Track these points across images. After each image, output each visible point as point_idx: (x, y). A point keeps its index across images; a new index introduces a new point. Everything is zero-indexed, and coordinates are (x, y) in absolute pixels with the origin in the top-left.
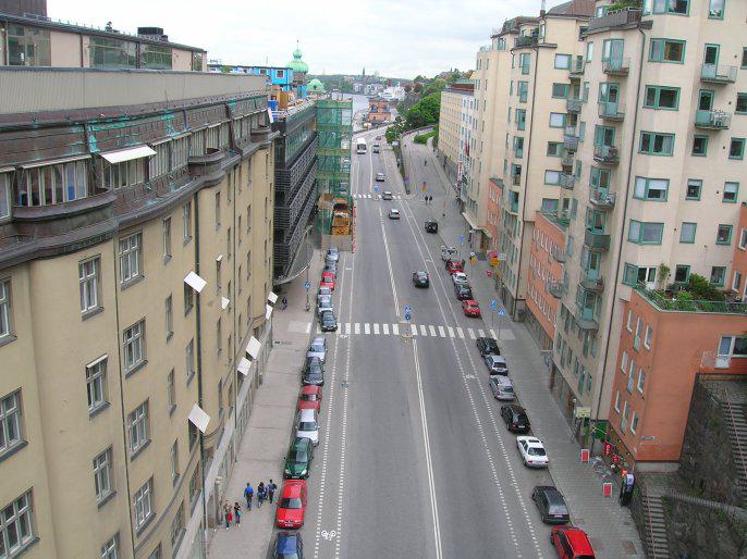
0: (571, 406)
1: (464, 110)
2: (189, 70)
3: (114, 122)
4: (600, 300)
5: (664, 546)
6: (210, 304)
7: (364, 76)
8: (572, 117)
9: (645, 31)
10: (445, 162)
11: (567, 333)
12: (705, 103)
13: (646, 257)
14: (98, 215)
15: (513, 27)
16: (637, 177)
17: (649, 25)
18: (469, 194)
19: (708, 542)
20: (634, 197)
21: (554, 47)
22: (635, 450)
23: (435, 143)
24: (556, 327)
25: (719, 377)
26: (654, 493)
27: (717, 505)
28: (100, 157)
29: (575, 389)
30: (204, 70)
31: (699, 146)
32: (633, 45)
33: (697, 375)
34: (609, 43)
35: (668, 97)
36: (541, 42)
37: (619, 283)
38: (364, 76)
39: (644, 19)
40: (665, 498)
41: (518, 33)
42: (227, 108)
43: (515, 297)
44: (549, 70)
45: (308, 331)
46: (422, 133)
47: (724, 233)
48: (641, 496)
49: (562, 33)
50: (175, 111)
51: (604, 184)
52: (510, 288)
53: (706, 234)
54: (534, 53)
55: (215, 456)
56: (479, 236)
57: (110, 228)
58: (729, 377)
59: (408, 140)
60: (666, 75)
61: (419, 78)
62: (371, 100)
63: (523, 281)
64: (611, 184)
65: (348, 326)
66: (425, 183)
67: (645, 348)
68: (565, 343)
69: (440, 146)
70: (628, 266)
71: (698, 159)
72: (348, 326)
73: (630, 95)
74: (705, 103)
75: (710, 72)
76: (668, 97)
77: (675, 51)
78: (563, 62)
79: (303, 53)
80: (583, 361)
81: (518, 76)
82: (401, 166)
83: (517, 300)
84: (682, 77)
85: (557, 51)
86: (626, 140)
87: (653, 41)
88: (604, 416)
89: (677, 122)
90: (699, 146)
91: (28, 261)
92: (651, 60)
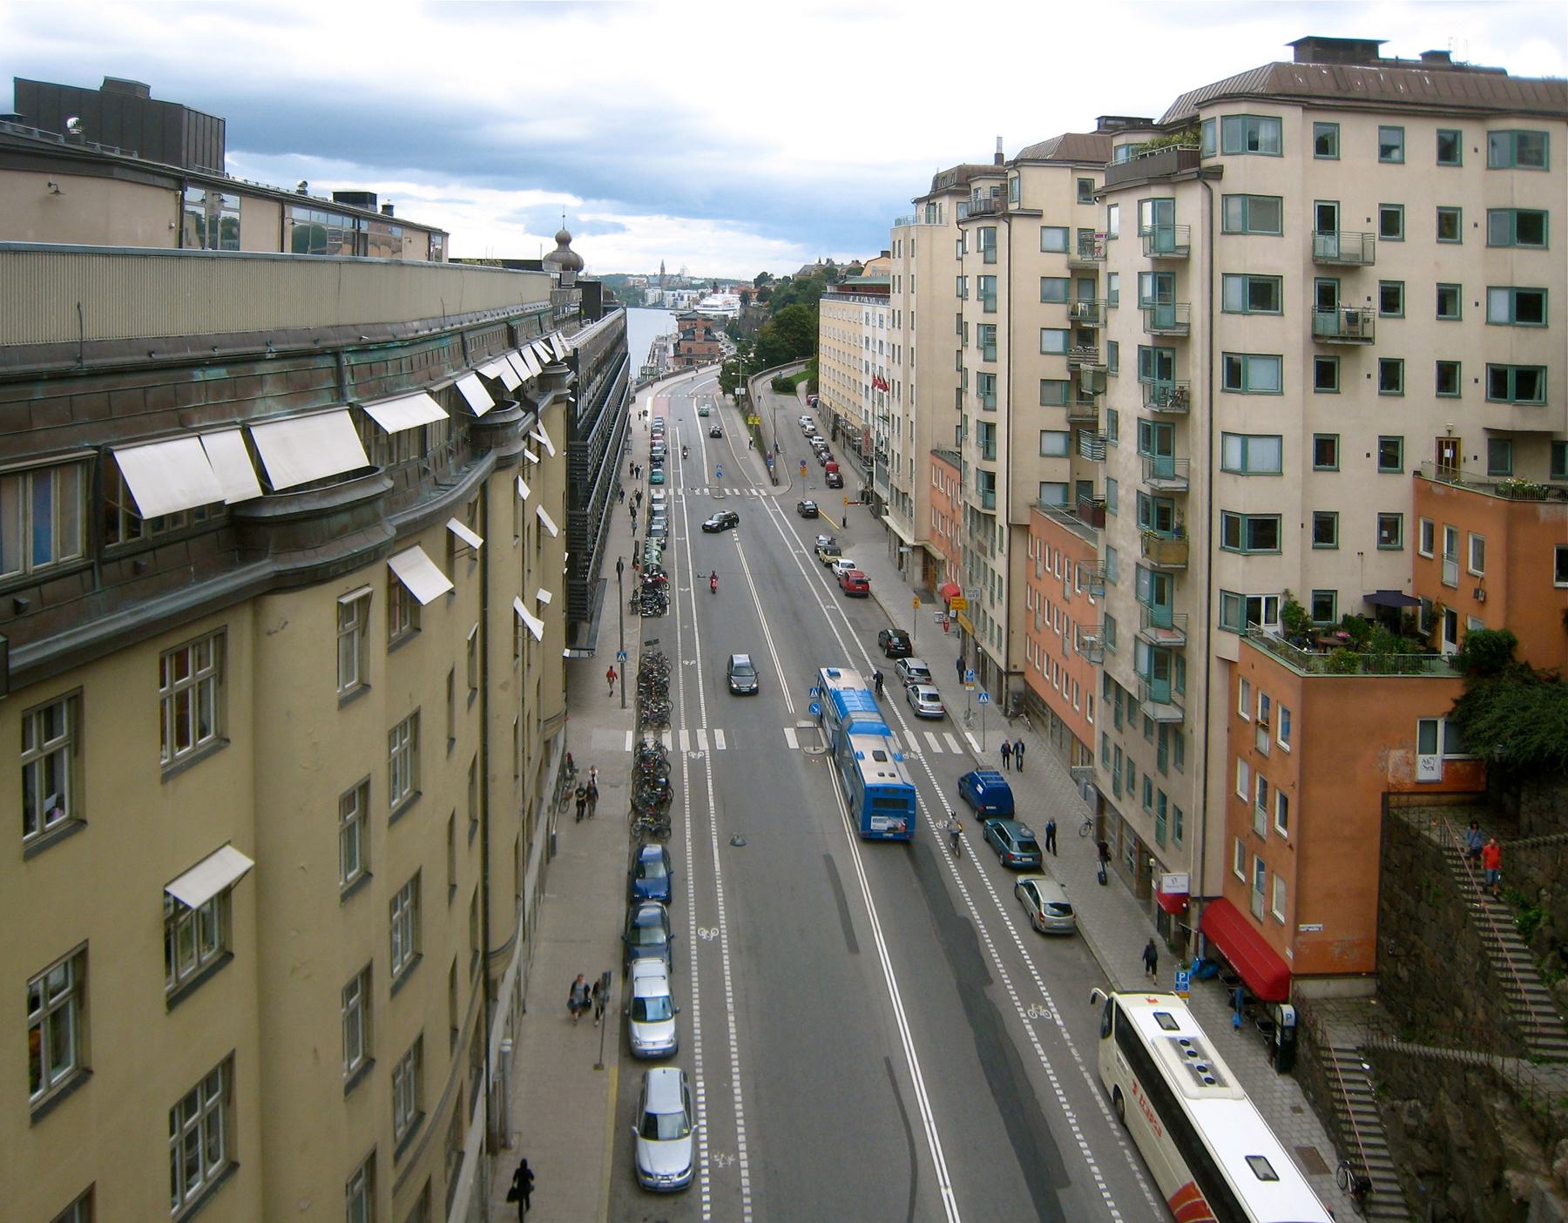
0: (1144, 874)
1: (867, 331)
3: (379, 349)
4: (1182, 663)
5: (1384, 1152)
6: (504, 687)
7: (663, 275)
8: (1082, 334)
9: (1213, 185)
10: (837, 427)
11: (1120, 730)
13: (1243, 574)
14: (366, 512)
15: (955, 183)
16: (1224, 433)
17: (1217, 173)
18: (894, 480)
19: (1473, 1136)
20: (1223, 470)
21: (1038, 215)
22: (1289, 953)
23: (814, 388)
24: (1098, 721)
25: (1426, 798)
26: (1341, 1038)
27: (1481, 1058)
28: (362, 409)
29: (1149, 839)
30: (445, 262)
32: (1190, 205)
33: (1385, 796)
34: (1148, 207)
35: (1263, 294)
36: (1013, 207)
37: (1214, 630)
38: (663, 275)
39: (1206, 163)
40: (1368, 1052)
41: (967, 193)
42: (510, 328)
43: (1003, 668)
44: (1032, 257)
45: (629, 746)
46: (787, 373)
47: (1389, 526)
48: (1318, 1048)
49: (1051, 191)
50: (283, 356)
51: (1166, 450)
52: (992, 652)
53: (1358, 531)
54: (1002, 228)
55: (499, 997)
56: (919, 558)
57: (386, 538)
58: (1445, 798)
59: (761, 386)
60: (1256, 255)
61: (763, 278)
62: (681, 318)
63: (1017, 637)
64: (1179, 451)
65: (702, 735)
66: (803, 463)
67: (1280, 748)
68: (1118, 749)
69: (824, 396)
70: (1227, 596)
71: (1326, 399)
72: (702, 735)
73: (1194, 295)
74: (1326, 298)
75: (1328, 246)
76: (1263, 294)
77: (1263, 213)
78: (1056, 240)
80: (1159, 782)
81: (974, 265)
82: (759, 441)
83: (1008, 673)
84: (1284, 256)
85: (1046, 222)
86: (1195, 371)
88: (1214, 888)
89: (1286, 333)
90: (1326, 377)
91: (255, 596)
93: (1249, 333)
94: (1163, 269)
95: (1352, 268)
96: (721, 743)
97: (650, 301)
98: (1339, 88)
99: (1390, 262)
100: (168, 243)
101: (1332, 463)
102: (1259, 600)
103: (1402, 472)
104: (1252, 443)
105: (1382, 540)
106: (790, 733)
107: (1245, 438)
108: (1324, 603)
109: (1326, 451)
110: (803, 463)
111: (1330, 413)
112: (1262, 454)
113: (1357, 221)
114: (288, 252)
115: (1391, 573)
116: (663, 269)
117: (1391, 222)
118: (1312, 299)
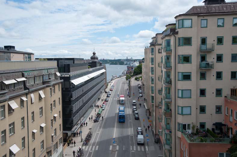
2: (23, 60)
7: (127, 59)
9: (176, 35)
12: (203, 58)
17: (177, 33)
31: (203, 76)
35: (187, 59)
37: (176, 131)
38: (127, 59)
60: (184, 50)
66: (134, 93)
70: (179, 124)
71: (203, 81)
74: (203, 58)
75: (204, 47)
76: (187, 59)
79: (96, 52)
84: (192, 50)
87: (179, 39)
89: (192, 68)
90: (203, 76)
92: (179, 45)
93: (184, 68)
94: (168, 55)
95: (210, 51)
96: (97, 149)
97: (125, 63)
98: (208, 11)
99: (219, 50)
100: (23, 60)
101: (204, 95)
102: (186, 125)
103: (222, 96)
104: (183, 91)
105: (217, 111)
106: (111, 147)
107: (182, 90)
108: (203, 125)
109: (203, 92)
110: (134, 93)
111: (203, 84)
112: (186, 94)
113: (211, 41)
114: (27, 61)
115: (219, 118)
116: (127, 58)
117: (220, 41)
118: (199, 60)
